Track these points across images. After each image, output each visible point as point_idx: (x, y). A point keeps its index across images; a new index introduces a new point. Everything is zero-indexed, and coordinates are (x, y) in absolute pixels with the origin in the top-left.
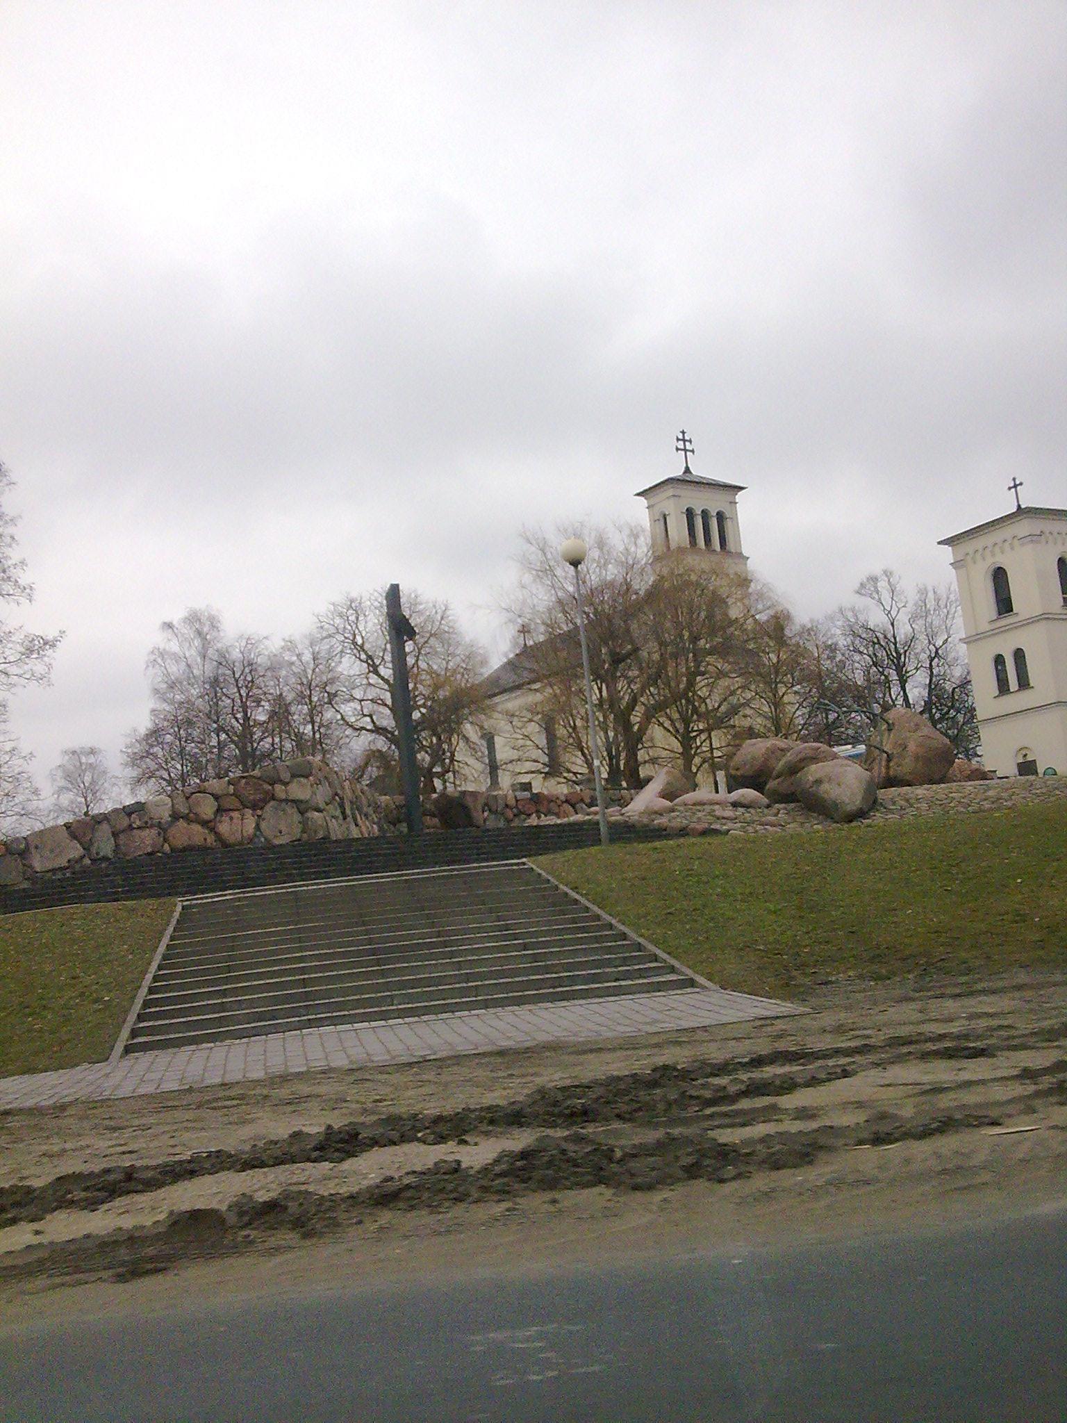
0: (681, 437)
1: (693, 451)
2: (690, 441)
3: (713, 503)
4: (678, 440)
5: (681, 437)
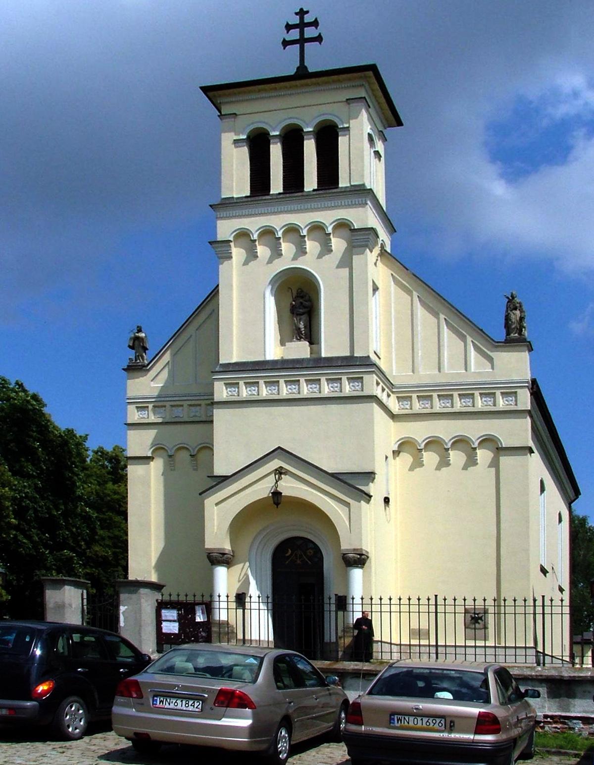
0: (296, 20)
1: (319, 39)
2: (315, 24)
3: (308, 111)
4: (289, 27)
5: (296, 20)
